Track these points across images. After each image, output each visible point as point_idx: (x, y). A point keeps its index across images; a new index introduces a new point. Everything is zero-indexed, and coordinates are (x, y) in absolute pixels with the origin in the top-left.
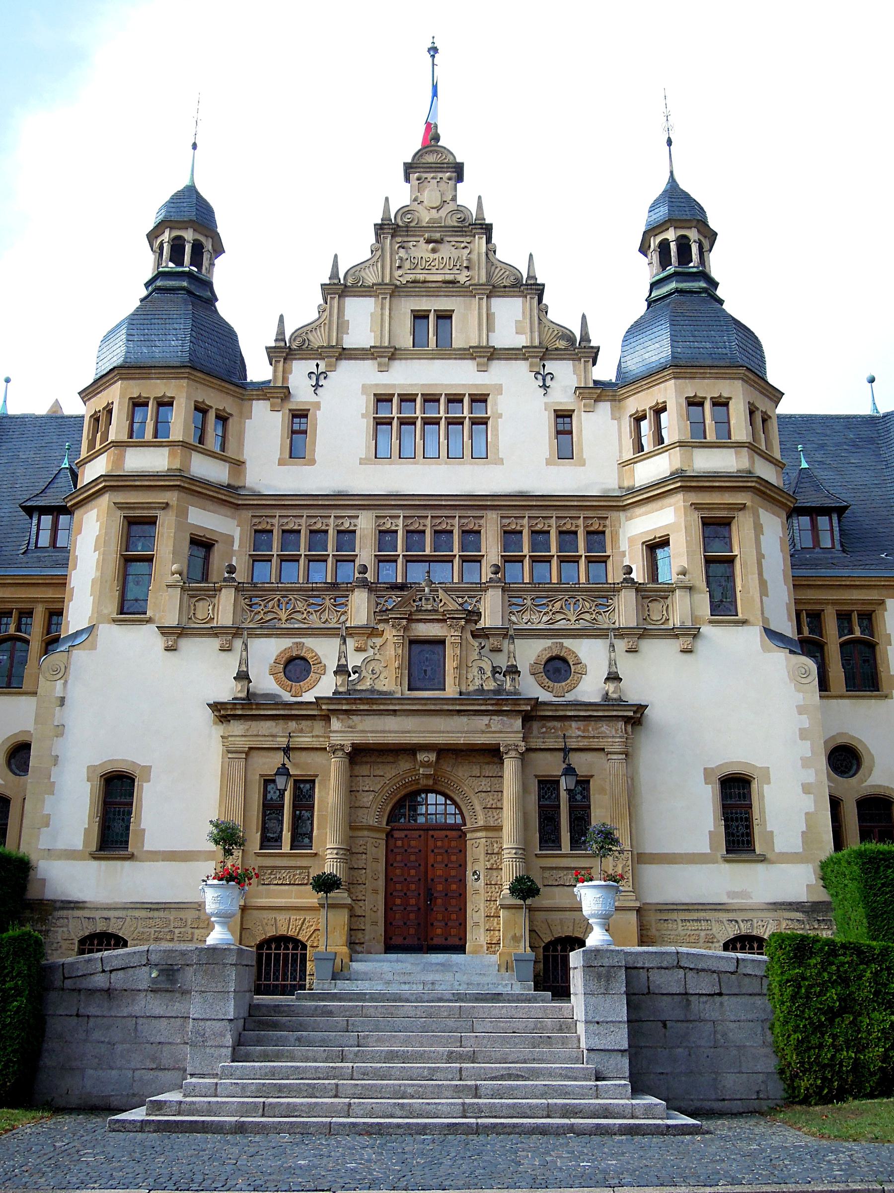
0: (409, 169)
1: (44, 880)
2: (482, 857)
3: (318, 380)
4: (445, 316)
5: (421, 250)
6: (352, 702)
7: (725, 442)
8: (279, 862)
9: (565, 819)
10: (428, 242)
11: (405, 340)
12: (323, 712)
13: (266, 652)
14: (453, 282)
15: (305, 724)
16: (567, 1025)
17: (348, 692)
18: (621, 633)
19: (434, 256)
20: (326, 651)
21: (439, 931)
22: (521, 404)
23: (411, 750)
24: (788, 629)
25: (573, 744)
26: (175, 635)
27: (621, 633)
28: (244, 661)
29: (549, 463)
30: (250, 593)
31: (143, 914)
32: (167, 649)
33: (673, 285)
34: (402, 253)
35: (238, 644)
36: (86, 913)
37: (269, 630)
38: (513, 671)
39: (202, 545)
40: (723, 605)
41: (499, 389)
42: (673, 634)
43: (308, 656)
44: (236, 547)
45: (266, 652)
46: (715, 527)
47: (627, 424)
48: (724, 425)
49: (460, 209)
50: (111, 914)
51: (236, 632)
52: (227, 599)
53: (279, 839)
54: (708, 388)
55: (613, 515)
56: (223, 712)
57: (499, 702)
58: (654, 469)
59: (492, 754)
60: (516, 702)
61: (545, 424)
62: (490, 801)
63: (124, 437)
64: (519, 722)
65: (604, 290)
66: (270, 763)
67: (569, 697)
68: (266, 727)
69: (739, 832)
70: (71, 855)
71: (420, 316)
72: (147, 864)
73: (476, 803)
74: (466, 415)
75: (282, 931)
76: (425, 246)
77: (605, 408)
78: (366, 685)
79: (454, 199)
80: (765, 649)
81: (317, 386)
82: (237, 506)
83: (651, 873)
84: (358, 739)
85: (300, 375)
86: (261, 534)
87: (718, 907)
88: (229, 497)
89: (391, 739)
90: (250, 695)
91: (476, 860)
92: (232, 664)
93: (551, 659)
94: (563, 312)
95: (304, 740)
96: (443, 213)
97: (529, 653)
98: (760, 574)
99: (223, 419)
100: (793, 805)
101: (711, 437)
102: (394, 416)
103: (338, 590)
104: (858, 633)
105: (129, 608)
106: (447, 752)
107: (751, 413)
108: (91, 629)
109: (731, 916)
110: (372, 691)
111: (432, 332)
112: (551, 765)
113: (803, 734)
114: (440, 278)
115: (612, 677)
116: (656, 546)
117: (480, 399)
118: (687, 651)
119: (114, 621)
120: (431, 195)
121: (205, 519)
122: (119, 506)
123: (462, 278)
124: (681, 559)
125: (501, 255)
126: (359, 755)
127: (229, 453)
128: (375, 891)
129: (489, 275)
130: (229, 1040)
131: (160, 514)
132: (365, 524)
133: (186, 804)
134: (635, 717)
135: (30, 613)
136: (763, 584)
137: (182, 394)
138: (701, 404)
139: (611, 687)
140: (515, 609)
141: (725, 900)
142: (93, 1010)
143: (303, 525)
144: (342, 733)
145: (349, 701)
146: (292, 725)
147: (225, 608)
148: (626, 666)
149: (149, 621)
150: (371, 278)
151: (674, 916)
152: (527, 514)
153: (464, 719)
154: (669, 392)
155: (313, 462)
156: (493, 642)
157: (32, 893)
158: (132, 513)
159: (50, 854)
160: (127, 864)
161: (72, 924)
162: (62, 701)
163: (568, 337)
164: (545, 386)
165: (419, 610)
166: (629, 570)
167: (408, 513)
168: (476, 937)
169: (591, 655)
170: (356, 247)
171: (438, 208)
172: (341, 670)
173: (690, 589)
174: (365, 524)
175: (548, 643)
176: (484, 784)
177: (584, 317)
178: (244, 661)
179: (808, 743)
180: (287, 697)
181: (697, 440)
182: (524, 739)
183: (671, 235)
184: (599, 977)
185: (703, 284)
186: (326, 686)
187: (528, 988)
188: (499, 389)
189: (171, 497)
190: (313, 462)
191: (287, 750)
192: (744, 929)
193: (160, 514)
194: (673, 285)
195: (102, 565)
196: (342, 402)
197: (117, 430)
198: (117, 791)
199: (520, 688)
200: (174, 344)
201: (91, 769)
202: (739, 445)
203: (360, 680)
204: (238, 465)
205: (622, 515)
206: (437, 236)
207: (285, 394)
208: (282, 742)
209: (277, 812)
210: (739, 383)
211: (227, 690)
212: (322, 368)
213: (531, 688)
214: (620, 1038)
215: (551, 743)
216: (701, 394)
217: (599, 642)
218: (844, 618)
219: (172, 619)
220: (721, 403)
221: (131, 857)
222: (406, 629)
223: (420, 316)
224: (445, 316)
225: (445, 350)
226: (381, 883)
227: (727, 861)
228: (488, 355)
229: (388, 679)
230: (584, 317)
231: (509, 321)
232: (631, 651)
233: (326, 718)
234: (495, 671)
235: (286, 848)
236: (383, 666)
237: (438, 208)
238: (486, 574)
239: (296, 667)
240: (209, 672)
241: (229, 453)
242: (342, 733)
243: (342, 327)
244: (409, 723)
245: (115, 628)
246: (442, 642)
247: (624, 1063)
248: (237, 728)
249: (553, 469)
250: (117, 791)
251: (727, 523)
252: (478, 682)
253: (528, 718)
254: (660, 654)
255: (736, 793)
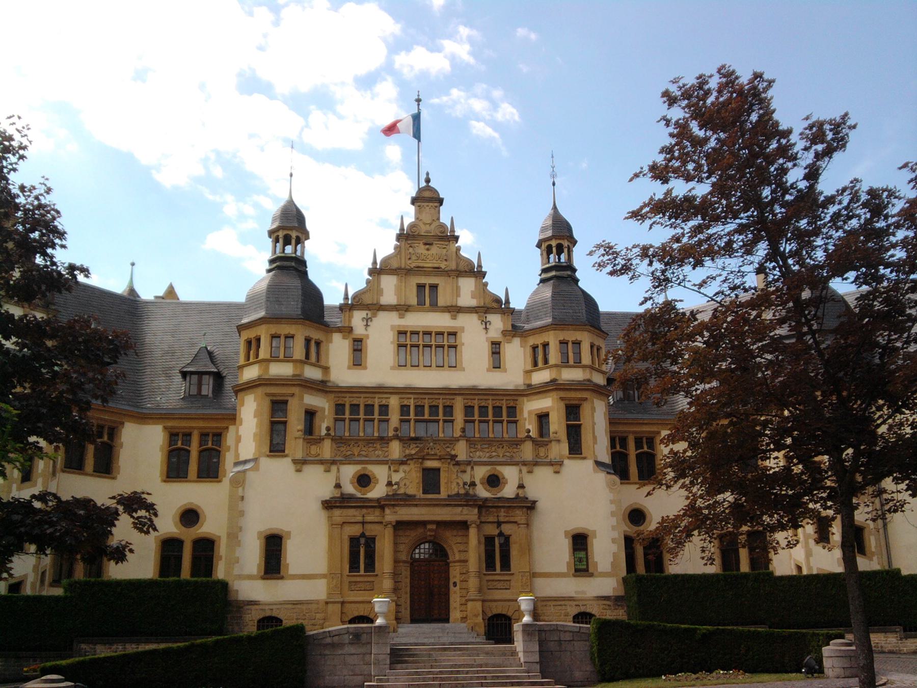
0: (414, 201)
1: (237, 591)
2: (458, 575)
3: (367, 321)
4: (434, 287)
5: (421, 249)
6: (395, 499)
7: (578, 363)
8: (358, 579)
9: (498, 555)
10: (425, 244)
11: (414, 301)
12: (380, 505)
13: (349, 472)
14: (438, 268)
15: (370, 510)
16: (514, 653)
17: (393, 495)
18: (524, 463)
19: (426, 255)
20: (380, 473)
21: (436, 612)
22: (475, 338)
23: (424, 523)
24: (606, 458)
25: (501, 519)
26: (300, 464)
27: (524, 463)
28: (338, 478)
29: (488, 370)
30: (339, 441)
31: (290, 606)
32: (299, 471)
33: (553, 273)
34: (411, 250)
35: (334, 468)
36: (261, 607)
37: (348, 460)
38: (473, 484)
39: (310, 414)
40: (576, 449)
41: (462, 329)
42: (551, 464)
43: (369, 474)
44: (326, 413)
45: (349, 472)
46: (573, 411)
47: (529, 351)
48: (578, 354)
49: (443, 226)
50: (274, 607)
51: (334, 462)
52: (327, 445)
53: (358, 567)
54: (571, 335)
55: (520, 399)
56: (328, 505)
57: (467, 501)
58: (541, 377)
59: (464, 525)
60: (475, 501)
61: (486, 349)
62: (462, 548)
63: (269, 357)
64: (476, 511)
65: (517, 277)
66: (356, 530)
67: (499, 495)
68: (351, 512)
69: (582, 566)
70: (250, 577)
71: (420, 287)
72: (290, 581)
73: (454, 547)
74: (445, 344)
75: (362, 614)
76: (423, 246)
77: (517, 341)
78: (401, 491)
79: (438, 219)
80: (595, 471)
81: (367, 325)
82: (326, 392)
83: (539, 582)
84: (399, 518)
85: (357, 318)
86: (339, 409)
87: (571, 599)
88: (322, 387)
89: (415, 518)
90: (342, 494)
91: (455, 577)
92: (331, 479)
93: (490, 476)
94: (496, 287)
95: (369, 518)
96: (433, 226)
97: (481, 472)
98: (594, 433)
99: (318, 344)
100: (606, 551)
101: (571, 362)
102: (410, 344)
103: (384, 440)
104: (646, 449)
105: (276, 448)
106: (439, 523)
107: (592, 347)
108: (255, 460)
109: (575, 603)
110: (405, 494)
111: (427, 297)
112: (492, 530)
113: (613, 514)
114: (430, 265)
115: (521, 486)
116: (543, 418)
117: (454, 334)
118: (557, 472)
119: (268, 456)
120: (426, 218)
121: (313, 400)
122: (268, 395)
123: (443, 266)
124: (557, 424)
125: (463, 253)
126: (400, 526)
127: (323, 363)
128: (406, 593)
129: (457, 265)
130: (388, 662)
131: (290, 399)
132: (394, 402)
133: (312, 553)
134: (530, 506)
135: (190, 435)
136: (595, 438)
137: (300, 333)
138: (567, 343)
139: (520, 491)
140: (472, 450)
141: (573, 595)
142: (327, 652)
143: (362, 402)
144: (390, 516)
145: (394, 500)
146: (364, 511)
147: (327, 450)
148: (528, 480)
149: (286, 456)
150: (395, 265)
151: (549, 603)
152: (477, 397)
153: (449, 509)
154: (553, 339)
155: (365, 368)
156: (462, 467)
157: (232, 597)
158: (275, 398)
159: (241, 577)
160: (280, 581)
161: (253, 612)
162: (242, 498)
163: (498, 300)
164: (486, 328)
165: (428, 454)
166: (529, 431)
167: (416, 396)
168: (455, 614)
169: (510, 474)
170: (387, 246)
171: (430, 224)
172: (389, 484)
173: (559, 441)
174: (394, 402)
175: (489, 468)
176: (459, 539)
177: (507, 289)
178: (338, 478)
179: (615, 519)
180: (359, 495)
181: (565, 363)
182: (479, 518)
183: (554, 243)
184: (528, 634)
185: (569, 273)
186: (378, 491)
187: (482, 639)
188: (462, 329)
189: (295, 390)
190: (365, 368)
191: (363, 523)
192: (582, 609)
193: (290, 399)
194: (553, 273)
195: (259, 425)
196: (380, 334)
197: (264, 353)
198: (274, 545)
199: (477, 493)
200: (294, 306)
201: (260, 533)
202: (585, 367)
203: (399, 488)
204: (326, 369)
205: (525, 399)
206: (430, 241)
207: (350, 330)
208: (360, 519)
209: (359, 554)
210: (586, 333)
211: (327, 491)
212: (369, 316)
213: (482, 492)
214: (536, 658)
215: (491, 519)
216: (567, 339)
217: (514, 467)
218: (639, 443)
219: (299, 455)
220: (577, 343)
221: (282, 578)
222: (421, 463)
223: (420, 287)
224: (434, 287)
225: (434, 306)
226: (408, 589)
227: (574, 576)
228: (455, 310)
229: (413, 487)
230: (507, 289)
231: (466, 289)
232: (530, 472)
233: (382, 508)
234: (465, 484)
235: (362, 572)
236: (409, 480)
237: (430, 224)
238: (458, 433)
239: (364, 480)
240: (319, 483)
241: (323, 363)
242: (390, 516)
243: (380, 292)
244: (424, 510)
245: (268, 459)
246: (438, 470)
247: (538, 667)
248: (337, 512)
249: (491, 374)
250: (274, 545)
251: (578, 407)
252: (456, 490)
253: (480, 507)
254: (543, 473)
255: (580, 541)
